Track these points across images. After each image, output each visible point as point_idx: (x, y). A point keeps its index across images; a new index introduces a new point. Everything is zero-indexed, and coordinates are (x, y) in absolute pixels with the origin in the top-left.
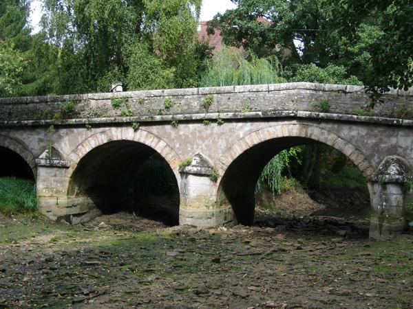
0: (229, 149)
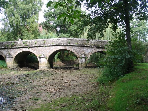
0: (49, 52)
